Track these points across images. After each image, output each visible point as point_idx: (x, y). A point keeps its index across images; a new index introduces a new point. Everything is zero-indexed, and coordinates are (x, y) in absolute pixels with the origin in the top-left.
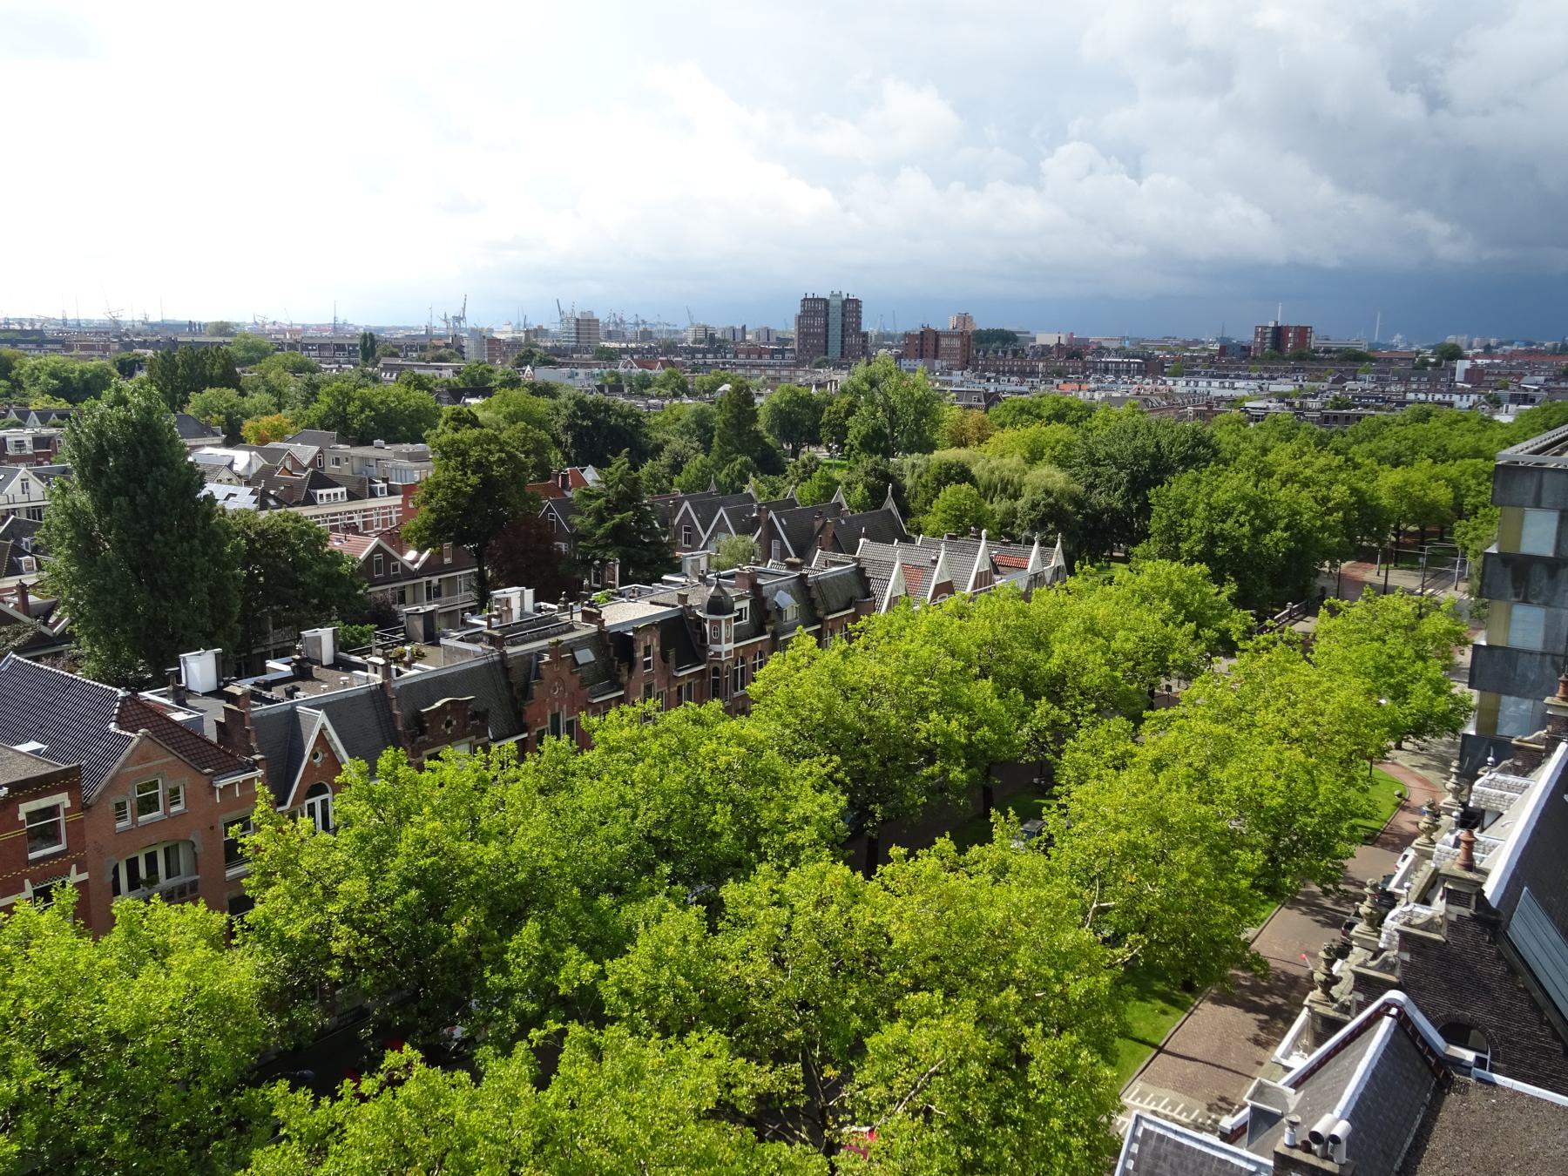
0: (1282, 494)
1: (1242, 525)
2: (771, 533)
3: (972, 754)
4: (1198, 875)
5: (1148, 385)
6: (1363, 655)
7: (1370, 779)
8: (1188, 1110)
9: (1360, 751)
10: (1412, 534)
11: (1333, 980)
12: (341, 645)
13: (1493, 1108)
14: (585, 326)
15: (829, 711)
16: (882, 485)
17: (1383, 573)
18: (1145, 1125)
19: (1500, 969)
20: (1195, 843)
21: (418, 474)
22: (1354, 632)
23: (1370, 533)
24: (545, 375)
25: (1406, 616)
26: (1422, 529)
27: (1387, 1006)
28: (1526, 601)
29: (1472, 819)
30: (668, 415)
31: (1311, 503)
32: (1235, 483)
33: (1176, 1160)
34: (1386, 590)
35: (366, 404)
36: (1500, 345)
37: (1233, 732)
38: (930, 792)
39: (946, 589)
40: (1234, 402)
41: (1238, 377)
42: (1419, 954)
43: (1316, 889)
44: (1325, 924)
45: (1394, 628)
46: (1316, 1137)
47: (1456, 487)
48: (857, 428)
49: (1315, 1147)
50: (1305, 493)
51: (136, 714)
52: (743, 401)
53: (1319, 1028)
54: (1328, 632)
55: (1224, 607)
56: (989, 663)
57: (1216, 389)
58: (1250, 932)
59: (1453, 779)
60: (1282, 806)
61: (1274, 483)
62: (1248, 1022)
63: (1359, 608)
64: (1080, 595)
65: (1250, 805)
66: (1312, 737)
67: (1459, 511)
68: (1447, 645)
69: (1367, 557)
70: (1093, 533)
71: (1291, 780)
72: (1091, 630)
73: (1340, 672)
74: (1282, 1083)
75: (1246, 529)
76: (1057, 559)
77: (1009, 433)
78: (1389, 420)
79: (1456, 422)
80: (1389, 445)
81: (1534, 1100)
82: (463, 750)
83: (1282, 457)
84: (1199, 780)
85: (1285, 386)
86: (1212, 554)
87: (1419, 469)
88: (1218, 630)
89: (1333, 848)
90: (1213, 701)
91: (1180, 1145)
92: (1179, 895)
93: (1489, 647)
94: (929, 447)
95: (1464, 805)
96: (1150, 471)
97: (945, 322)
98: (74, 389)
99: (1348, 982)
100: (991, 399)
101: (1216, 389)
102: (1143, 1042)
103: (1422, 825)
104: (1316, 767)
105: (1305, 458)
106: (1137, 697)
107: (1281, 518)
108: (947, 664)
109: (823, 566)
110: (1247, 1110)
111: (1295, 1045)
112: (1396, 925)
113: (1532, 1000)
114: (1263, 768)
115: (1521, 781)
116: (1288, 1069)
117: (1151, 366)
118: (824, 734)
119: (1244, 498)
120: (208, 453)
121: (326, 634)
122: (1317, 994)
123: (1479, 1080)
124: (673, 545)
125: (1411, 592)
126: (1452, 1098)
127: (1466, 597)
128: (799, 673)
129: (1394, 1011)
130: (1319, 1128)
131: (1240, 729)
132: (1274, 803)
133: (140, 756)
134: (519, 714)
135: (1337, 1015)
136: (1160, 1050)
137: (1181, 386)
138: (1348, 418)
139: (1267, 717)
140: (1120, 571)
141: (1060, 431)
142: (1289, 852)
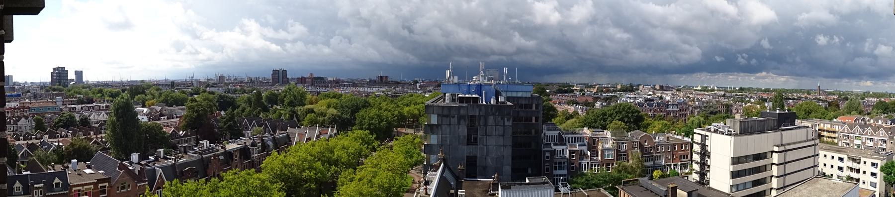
2: (266, 127)
3: (317, 181)
5: (354, 89)
9: (403, 172)
12: (165, 153)
14: (222, 77)
15: (281, 171)
16: (293, 114)
21: (183, 113)
24: (212, 89)
29: (427, 183)
30: (241, 98)
35: (172, 97)
38: (306, 191)
39: (309, 139)
48: (286, 100)
51: (122, 167)
52: (259, 94)
56: (320, 157)
57: (369, 90)
63: (401, 139)
64: (341, 139)
67: (420, 115)
69: (403, 127)
70: (343, 125)
72: (343, 148)
76: (335, 131)
77: (323, 101)
82: (193, 181)
83: (384, 105)
85: (383, 89)
94: (304, 105)
96: (355, 109)
97: (307, 75)
98: (114, 95)
100: (318, 93)
101: (369, 90)
106: (354, 164)
108: (310, 158)
109: (279, 134)
114: (383, 177)
117: (355, 85)
118: (280, 177)
120: (139, 109)
121: (162, 151)
124: (243, 130)
128: (274, 161)
133: (122, 176)
134: (206, 172)
137: (361, 89)
139: (384, 166)
140: (350, 133)
141: (335, 100)
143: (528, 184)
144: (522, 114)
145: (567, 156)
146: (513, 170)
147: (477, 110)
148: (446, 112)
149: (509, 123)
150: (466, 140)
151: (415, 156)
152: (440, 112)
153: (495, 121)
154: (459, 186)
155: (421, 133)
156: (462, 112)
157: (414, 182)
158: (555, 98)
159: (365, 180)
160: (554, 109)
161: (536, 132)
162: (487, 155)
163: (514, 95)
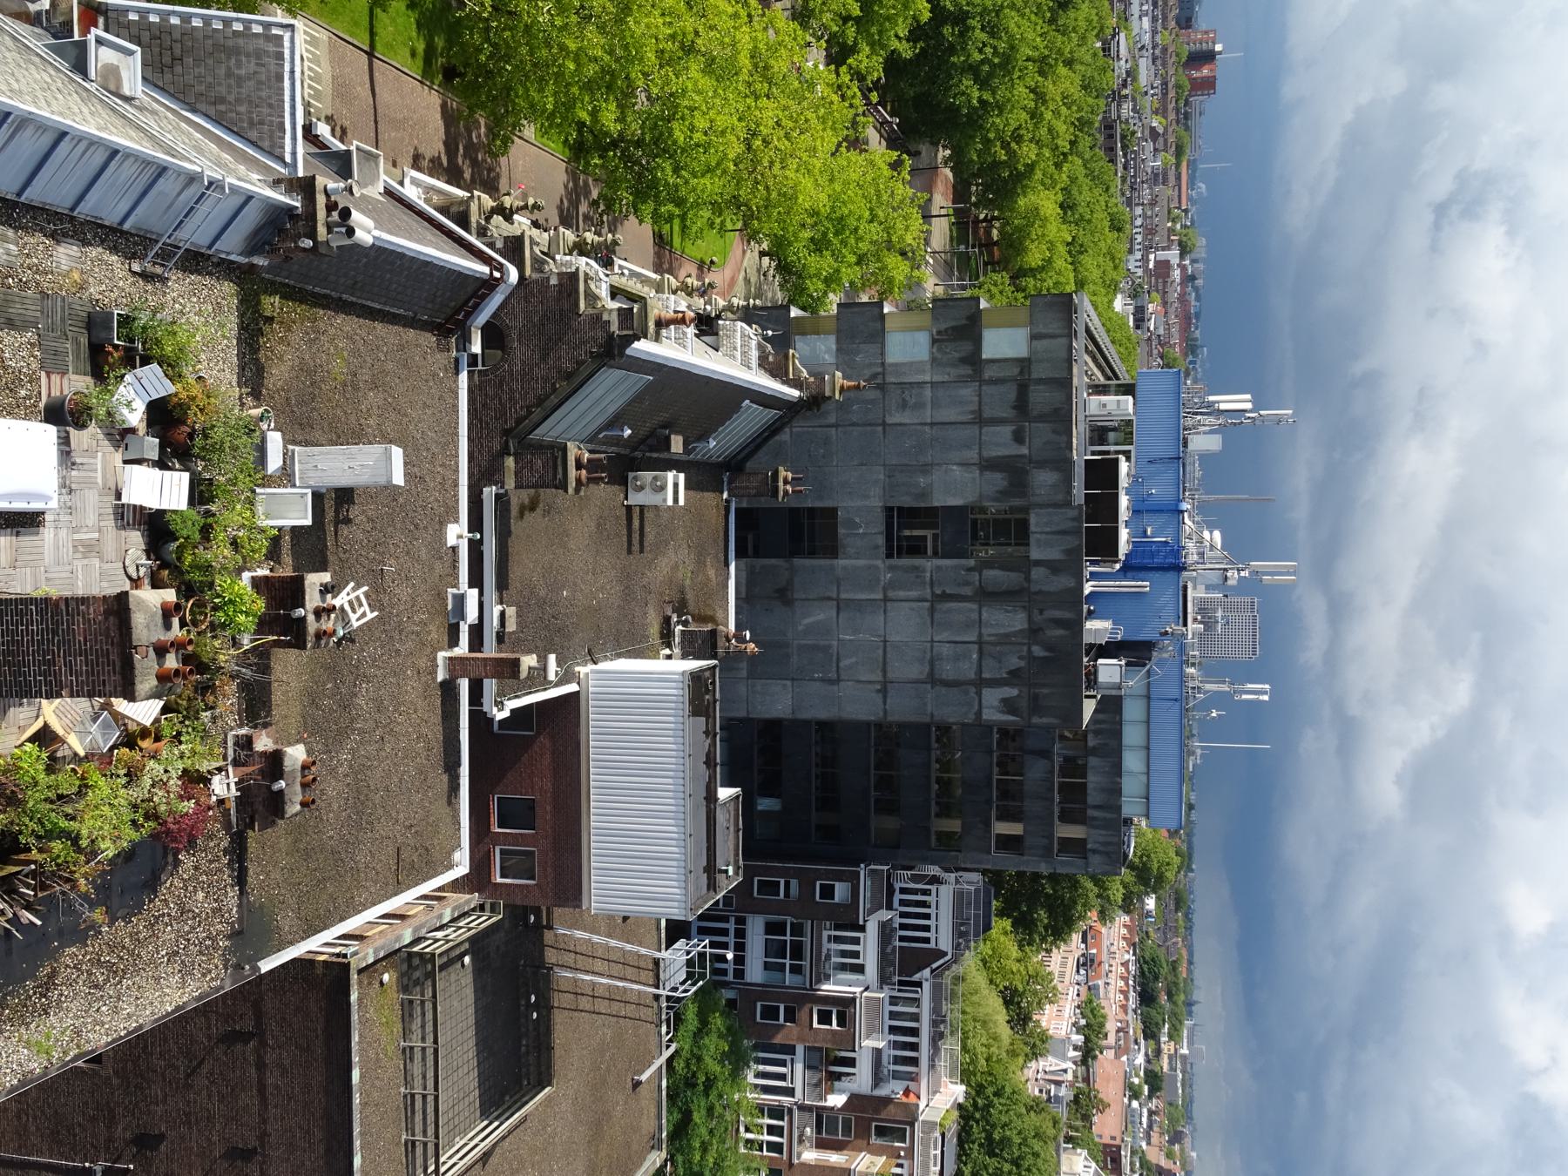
0: (1021, 90)
1: (981, 51)
4: (577, 60)
6: (853, 202)
7: (723, 230)
8: (317, 95)
10: (988, 233)
11: (508, 215)
13: (435, 375)
17: (943, 212)
18: (287, 36)
19: (568, 366)
20: (611, 52)
22: (878, 191)
23: (984, 192)
25: (901, 238)
26: (996, 243)
27: (500, 268)
28: (934, 341)
29: (706, 325)
31: (1014, 124)
32: (1030, 35)
33: (263, 78)
34: (927, 217)
36: (1196, 289)
37: (744, 76)
40: (1125, 18)
41: (1154, 20)
42: (560, 292)
43: (595, 194)
44: (560, 208)
45: (887, 230)
46: (346, 214)
47: (1042, 269)
49: (335, 214)
50: (1024, 116)
53: (454, 209)
54: (872, 163)
55: (883, 47)
58: (529, 131)
59: (742, 303)
60: (675, 142)
61: (1033, 78)
62: (434, 145)
63: (903, 191)
65: (670, 106)
66: (755, 162)
68: (875, 283)
71: (706, 147)
73: (831, 181)
74: (384, 179)
75: (977, 57)
78: (1112, 190)
79: (1113, 259)
80: (1084, 196)
81: (455, 408)
83: (1065, 82)
84: (682, 47)
86: (943, 23)
87: (1059, 230)
88: (855, 43)
89: (644, 202)
90: (773, 49)
91: (280, 78)
92: (549, 46)
93: (882, 317)
95: (718, 317)
99: (514, 230)
102: (372, 34)
103: (689, 280)
104: (725, 172)
105: (1064, 110)
107: (994, 93)
110: (344, 147)
111: (429, 189)
112: (583, 268)
113: (547, 397)
114: (713, 115)
115: (754, 362)
116: (401, 183)
119: (1012, 47)
122: (488, 202)
123: (457, 360)
125: (927, 242)
126: (429, 339)
127: (929, 295)
129: (497, 274)
130: (356, 216)
131: (749, 85)
132: (677, 133)
135: (474, 225)
136: (371, 55)
138: (1110, 150)
142: (626, 158)
143: (711, 797)
144: (1035, 771)
145: (828, 988)
146: (773, 729)
147: (1054, 554)
148: (1040, 398)
149: (992, 706)
150: (907, 501)
151: (825, 263)
152: (1038, 372)
153: (1005, 639)
154: (703, 476)
155: (932, 286)
156: (1044, 479)
157: (703, 266)
158: (1114, 937)
159: (689, 23)
160: (1059, 931)
161: (946, 839)
162: (840, 605)
163: (1132, 735)
